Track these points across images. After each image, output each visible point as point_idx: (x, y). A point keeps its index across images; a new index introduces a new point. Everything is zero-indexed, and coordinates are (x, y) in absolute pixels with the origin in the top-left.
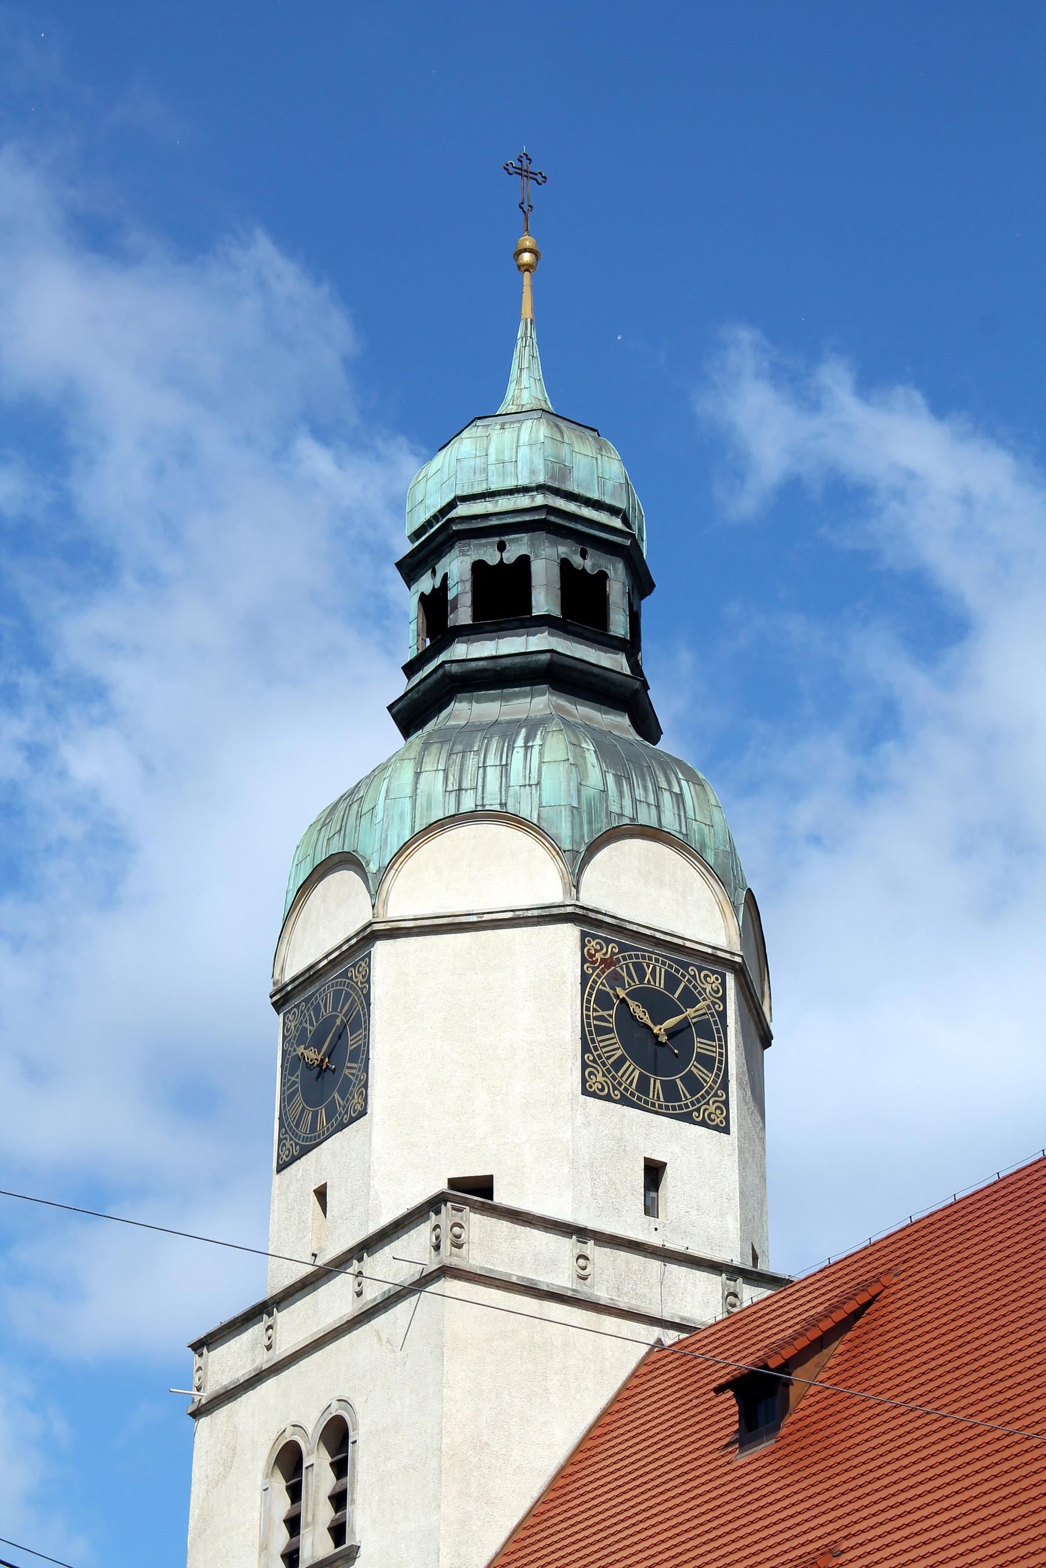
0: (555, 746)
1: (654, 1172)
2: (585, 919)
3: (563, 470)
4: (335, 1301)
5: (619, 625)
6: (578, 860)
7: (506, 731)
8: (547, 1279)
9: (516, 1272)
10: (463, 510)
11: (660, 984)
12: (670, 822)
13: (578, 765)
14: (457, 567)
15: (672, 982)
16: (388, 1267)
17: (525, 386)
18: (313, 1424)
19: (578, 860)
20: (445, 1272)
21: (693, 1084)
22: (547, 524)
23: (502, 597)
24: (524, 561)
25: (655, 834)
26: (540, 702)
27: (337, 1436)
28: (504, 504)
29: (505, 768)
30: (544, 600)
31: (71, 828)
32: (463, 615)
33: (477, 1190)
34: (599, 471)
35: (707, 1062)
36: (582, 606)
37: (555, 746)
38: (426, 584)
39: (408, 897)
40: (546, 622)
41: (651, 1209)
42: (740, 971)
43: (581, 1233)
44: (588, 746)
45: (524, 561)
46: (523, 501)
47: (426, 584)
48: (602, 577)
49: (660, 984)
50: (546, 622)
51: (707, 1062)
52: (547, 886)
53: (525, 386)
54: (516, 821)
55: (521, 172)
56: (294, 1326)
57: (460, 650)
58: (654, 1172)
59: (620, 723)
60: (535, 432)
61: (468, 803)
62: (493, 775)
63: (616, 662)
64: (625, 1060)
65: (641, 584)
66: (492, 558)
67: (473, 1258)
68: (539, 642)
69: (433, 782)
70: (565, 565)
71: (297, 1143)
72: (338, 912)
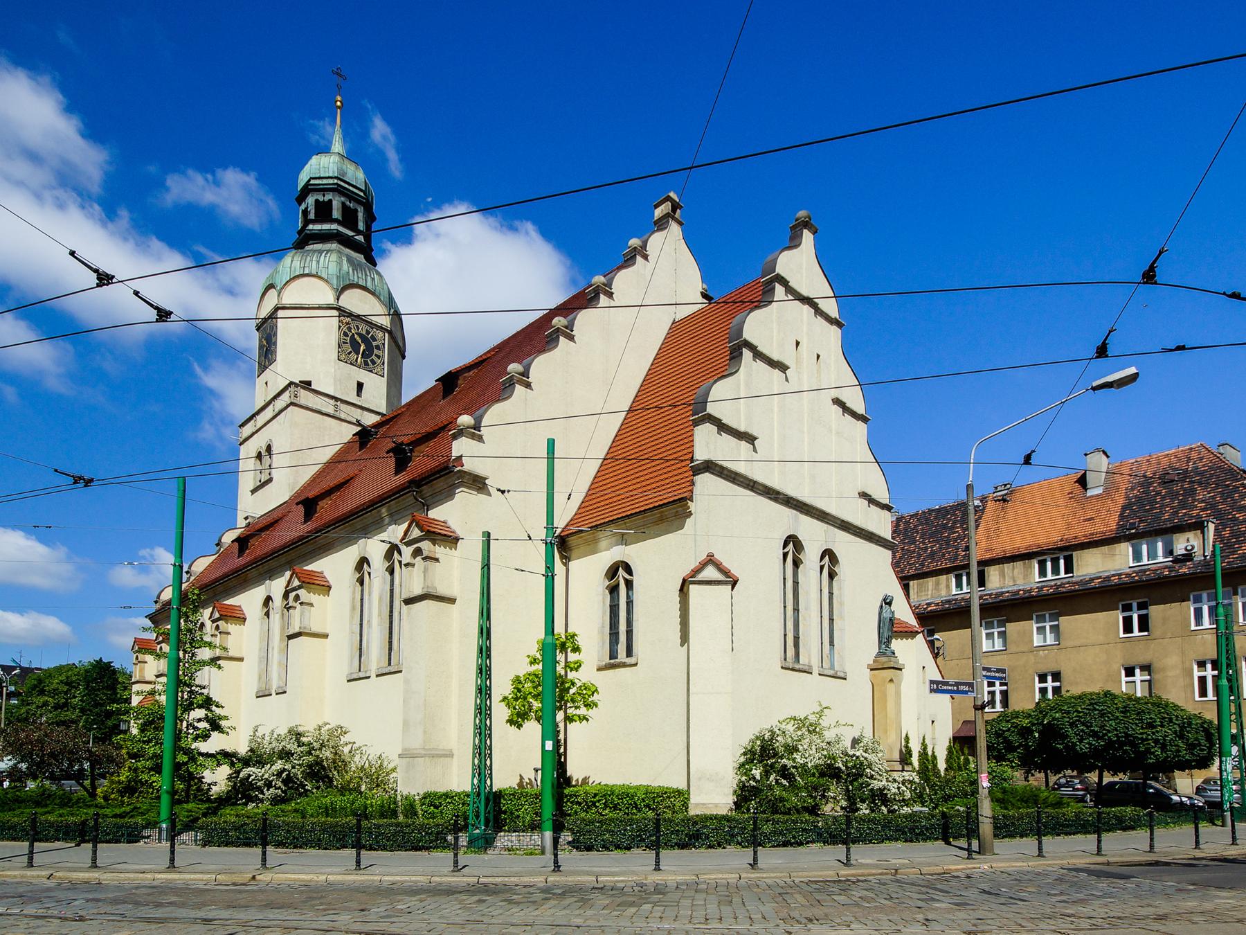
0: (334, 257)
1: (360, 386)
2: (342, 312)
3: (344, 174)
4: (268, 413)
5: (361, 226)
6: (340, 292)
7: (320, 252)
8: (324, 410)
9: (315, 407)
10: (312, 182)
11: (364, 332)
12: (369, 285)
13: (340, 263)
14: (311, 200)
15: (368, 332)
16: (280, 404)
17: (337, 146)
18: (264, 448)
19: (340, 292)
20: (292, 404)
21: (373, 362)
22: (339, 190)
23: (323, 212)
24: (330, 201)
25: (365, 288)
26: (334, 246)
27: (269, 448)
28: (325, 181)
29: (318, 262)
30: (336, 214)
31: (47, 194)
32: (312, 216)
33: (306, 385)
34: (356, 176)
35: (378, 357)
36: (349, 218)
37: (334, 257)
38: (303, 207)
39: (287, 299)
40: (336, 221)
41: (358, 395)
42: (390, 332)
43: (336, 399)
44: (345, 259)
45: (330, 201)
46: (331, 181)
47: (303, 207)
48: (356, 211)
49: (364, 332)
50: (336, 221)
51: (378, 357)
52: (329, 298)
53: (337, 146)
54: (321, 278)
55: (338, 74)
56: (261, 419)
57: (311, 227)
58: (360, 386)
59: (360, 258)
60: (337, 159)
61: (307, 271)
62: (314, 263)
63: (360, 238)
64: (1131, 618)
65: (370, 218)
66: (321, 198)
67: (302, 402)
68: (334, 226)
69: (297, 264)
70: (343, 204)
71: (263, 368)
72: (271, 300)
